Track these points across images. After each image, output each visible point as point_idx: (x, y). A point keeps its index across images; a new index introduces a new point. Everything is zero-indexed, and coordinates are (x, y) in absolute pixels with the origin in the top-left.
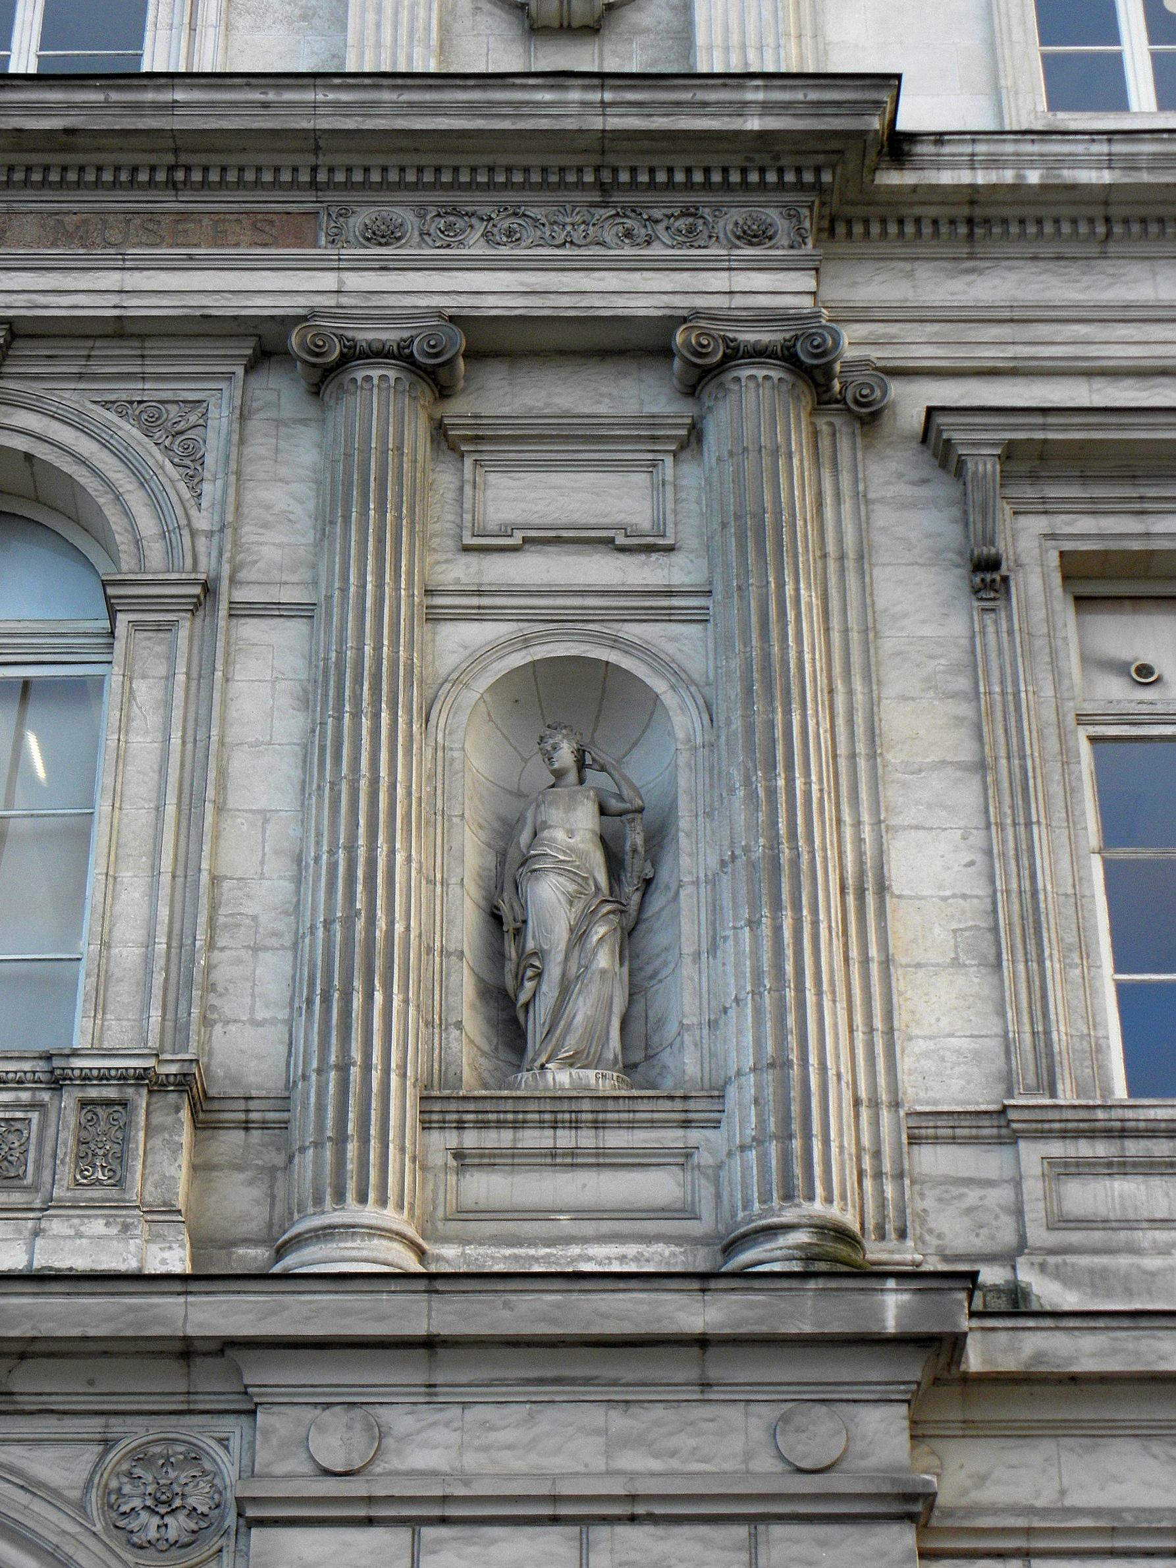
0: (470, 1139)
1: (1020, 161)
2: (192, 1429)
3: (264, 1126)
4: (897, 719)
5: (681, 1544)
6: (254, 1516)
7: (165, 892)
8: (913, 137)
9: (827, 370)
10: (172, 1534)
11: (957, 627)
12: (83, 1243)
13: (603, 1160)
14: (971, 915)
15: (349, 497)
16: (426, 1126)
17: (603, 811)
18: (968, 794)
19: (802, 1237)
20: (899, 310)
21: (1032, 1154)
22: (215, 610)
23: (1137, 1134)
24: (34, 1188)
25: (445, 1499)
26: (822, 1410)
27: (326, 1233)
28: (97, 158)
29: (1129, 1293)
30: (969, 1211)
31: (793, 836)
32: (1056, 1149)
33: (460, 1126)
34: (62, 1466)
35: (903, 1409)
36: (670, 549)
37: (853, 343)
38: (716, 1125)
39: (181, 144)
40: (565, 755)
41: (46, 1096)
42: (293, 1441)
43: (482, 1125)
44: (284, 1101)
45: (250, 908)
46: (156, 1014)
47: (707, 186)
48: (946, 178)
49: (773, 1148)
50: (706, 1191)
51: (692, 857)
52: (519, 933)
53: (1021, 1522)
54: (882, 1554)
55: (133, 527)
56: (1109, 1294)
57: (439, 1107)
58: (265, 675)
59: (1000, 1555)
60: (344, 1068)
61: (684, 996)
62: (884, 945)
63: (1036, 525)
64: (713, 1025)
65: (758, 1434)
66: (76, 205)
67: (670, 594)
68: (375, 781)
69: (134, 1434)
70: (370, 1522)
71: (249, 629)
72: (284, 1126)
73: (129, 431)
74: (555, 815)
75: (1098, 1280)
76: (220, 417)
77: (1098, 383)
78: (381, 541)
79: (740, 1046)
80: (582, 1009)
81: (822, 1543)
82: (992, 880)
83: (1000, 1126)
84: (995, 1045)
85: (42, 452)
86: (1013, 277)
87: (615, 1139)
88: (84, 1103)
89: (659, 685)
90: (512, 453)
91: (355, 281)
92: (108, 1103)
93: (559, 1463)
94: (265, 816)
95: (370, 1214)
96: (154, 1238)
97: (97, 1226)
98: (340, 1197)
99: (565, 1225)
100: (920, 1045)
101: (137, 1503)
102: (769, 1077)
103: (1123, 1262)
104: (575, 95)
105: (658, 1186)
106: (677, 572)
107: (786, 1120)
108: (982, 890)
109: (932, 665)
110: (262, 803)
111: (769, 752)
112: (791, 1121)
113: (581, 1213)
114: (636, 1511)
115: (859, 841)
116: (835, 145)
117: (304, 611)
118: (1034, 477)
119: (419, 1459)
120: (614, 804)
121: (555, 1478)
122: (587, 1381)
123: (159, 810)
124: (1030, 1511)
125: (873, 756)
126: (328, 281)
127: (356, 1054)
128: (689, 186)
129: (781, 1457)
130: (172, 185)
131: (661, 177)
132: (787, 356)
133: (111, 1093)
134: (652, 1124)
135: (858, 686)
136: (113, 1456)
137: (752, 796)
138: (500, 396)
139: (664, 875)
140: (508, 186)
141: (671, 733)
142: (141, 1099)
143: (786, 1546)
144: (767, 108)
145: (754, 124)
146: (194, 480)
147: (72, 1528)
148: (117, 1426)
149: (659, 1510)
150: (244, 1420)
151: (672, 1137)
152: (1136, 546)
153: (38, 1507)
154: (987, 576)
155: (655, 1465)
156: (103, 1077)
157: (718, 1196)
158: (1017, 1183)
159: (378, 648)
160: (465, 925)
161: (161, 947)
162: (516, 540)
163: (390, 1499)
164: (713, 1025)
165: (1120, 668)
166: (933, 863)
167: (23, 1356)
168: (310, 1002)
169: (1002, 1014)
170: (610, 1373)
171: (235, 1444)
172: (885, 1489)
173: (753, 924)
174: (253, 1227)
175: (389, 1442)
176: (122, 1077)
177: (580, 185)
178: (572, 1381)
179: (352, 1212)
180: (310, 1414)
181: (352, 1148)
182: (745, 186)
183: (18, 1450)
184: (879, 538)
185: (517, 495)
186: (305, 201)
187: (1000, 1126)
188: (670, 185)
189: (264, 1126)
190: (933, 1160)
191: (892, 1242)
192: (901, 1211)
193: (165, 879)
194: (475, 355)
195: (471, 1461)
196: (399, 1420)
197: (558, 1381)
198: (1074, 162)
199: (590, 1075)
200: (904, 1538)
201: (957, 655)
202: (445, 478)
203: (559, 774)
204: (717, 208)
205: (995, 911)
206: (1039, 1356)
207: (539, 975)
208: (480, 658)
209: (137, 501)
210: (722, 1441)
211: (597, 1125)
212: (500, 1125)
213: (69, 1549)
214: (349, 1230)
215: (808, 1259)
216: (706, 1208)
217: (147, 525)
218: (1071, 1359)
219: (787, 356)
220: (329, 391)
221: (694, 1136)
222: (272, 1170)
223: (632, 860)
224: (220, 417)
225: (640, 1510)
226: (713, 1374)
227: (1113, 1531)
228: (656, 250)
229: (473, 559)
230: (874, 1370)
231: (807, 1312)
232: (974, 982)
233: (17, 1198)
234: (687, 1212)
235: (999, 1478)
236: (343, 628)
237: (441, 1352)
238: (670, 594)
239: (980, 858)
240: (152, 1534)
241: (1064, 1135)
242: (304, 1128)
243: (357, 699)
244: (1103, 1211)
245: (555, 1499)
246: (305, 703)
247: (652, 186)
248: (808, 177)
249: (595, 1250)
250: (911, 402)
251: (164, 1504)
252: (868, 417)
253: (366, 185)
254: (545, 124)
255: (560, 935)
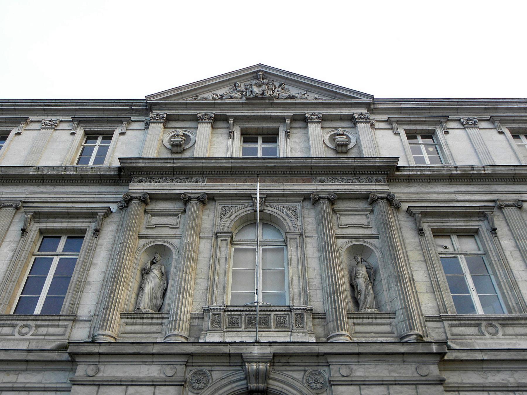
0: (355, 320)
1: (416, 171)
2: (318, 368)
3: (322, 318)
4: (410, 254)
5: (405, 388)
6: (332, 384)
7: (301, 281)
8: (400, 167)
9: (392, 201)
10: (318, 387)
11: (417, 240)
12: (298, 337)
13: (377, 324)
14: (428, 284)
15: (321, 220)
16: (348, 318)
17: (366, 268)
18: (424, 265)
19: (415, 336)
20: (401, 192)
21: (446, 323)
22: (303, 237)
23: (462, 320)
24: (289, 328)
25: (364, 381)
26: (423, 366)
27: (337, 336)
28: (278, 170)
29: (467, 346)
30: (437, 333)
31: (401, 271)
32: (450, 322)
33: (353, 318)
34: (298, 375)
35: (437, 365)
36: (371, 228)
37: (397, 197)
38: (395, 318)
39: (291, 168)
40: (359, 259)
41: (289, 313)
42: (337, 371)
43: (357, 318)
44: (325, 314)
45: (315, 283)
46: (302, 300)
47: (371, 174)
48: (405, 173)
49: (407, 322)
50: (395, 329)
51: (383, 275)
52: (357, 287)
53: (457, 385)
54: (438, 390)
55: (288, 225)
56: (464, 347)
57: (124, 315)
58: (312, 248)
59: (454, 391)
60: (335, 308)
61: (385, 297)
62: (415, 289)
63: (427, 224)
64: (391, 302)
65: (414, 370)
66: (275, 177)
67: (373, 234)
68: (333, 263)
69: (310, 370)
70: (352, 385)
71: (308, 240)
72: (325, 318)
73: (285, 210)
74: (360, 268)
75: (461, 344)
76: (299, 208)
77: (432, 203)
78: (328, 226)
79: (398, 305)
80: (369, 299)
81: (428, 388)
82: (430, 279)
83: (440, 319)
84: (436, 305)
85: (272, 213)
86: (416, 188)
87: (379, 320)
88: (296, 314)
89: (373, 248)
90: (345, 213)
91: (319, 188)
92: (300, 314)
93: (381, 375)
94: (315, 269)
95: (343, 332)
96: (310, 336)
97: (301, 334)
98: (338, 330)
99: (373, 335)
100: (424, 305)
101: (312, 381)
102: (404, 310)
103: (465, 341)
104: (350, 160)
105: (387, 328)
106: (373, 231)
107: (408, 317)
108: (429, 280)
109: (414, 246)
110: (314, 266)
111: (395, 258)
112: (409, 317)
113: (375, 333)
114: (396, 383)
115: (408, 273)
116: (390, 168)
117: (317, 237)
118: (425, 217)
119: (358, 374)
120: (368, 267)
121: (383, 377)
122: (385, 361)
123: (298, 267)
124: (457, 383)
125: (408, 259)
126: (315, 188)
127: (337, 306)
128: (368, 174)
129: (418, 373)
130: (290, 174)
131: (364, 173)
132: (387, 199)
133: (300, 312)
134: (384, 318)
135: (404, 248)
136: (307, 373)
137: (393, 265)
138: (341, 205)
139: (377, 278)
140: (341, 174)
141: (376, 256)
142: (305, 313)
143: (422, 389)
144: (379, 162)
145: (378, 165)
146: (296, 218)
147: (302, 386)
148: (307, 368)
149: (400, 383)
150: (327, 367)
151: (388, 320)
152: (442, 227)
153: (295, 382)
154: (421, 232)
155: (397, 375)
156: (298, 310)
157: (397, 330)
158: (444, 328)
159: (330, 242)
160: (348, 287)
161: (301, 289)
162: (347, 226)
163: (356, 381)
164: (391, 302)
165: (442, 246)
166: (420, 276)
167: (291, 356)
168: (327, 298)
169: (436, 300)
170: (388, 359)
171: (326, 371)
172: (437, 379)
173: (397, 285)
174: (322, 335)
175: (353, 371)
176: (302, 310)
177: (352, 174)
178: (382, 361)
179: (340, 332)
180: (339, 366)
181: (339, 321)
182: (376, 174)
183: (290, 372)
184: (402, 226)
185: (346, 220)
186: (310, 176)
187: (440, 319)
188: (365, 174)
189: (322, 318)
190: (429, 324)
191: (426, 338)
192: (426, 332)
193: (301, 278)
194: (338, 199)
195: (367, 374)
196: (354, 367)
197: (380, 360)
198: (425, 170)
199: (373, 310)
200: (441, 388)
201: (418, 244)
202: (334, 217)
203: (358, 262)
204: (372, 177)
205: (432, 284)
206: (456, 357)
207: (361, 294)
208: (344, 244)
209: (288, 221)
210: (407, 371)
211: (375, 318)
212: (360, 318)
213: (301, 389)
214: (341, 335)
215: (417, 340)
216: (395, 332)
217: (290, 224)
218: (461, 357)
219: (387, 199)
220: (316, 205)
221: (391, 320)
222: (324, 325)
223: (373, 275)
224: (299, 208)
225: (397, 383)
226: (405, 359)
227: (473, 387)
228: (363, 183)
229: (341, 229)
230: (432, 359)
231: (420, 349)
232: (430, 295)
233: (287, 329)
234: (392, 332)
235: (453, 378)
236: (324, 239)
237: (360, 356)
238: (373, 234)
239: (428, 276)
240: (315, 387)
241: (451, 320)
242: (330, 317)
243: (329, 250)
244: (459, 332)
245: (382, 381)
246: (318, 251)
247: (362, 174)
248: (386, 173)
249: (379, 339)
250: (405, 206)
251: (316, 382)
252: (397, 208)
253: (319, 174)
254: (346, 165)
255: (363, 288)
